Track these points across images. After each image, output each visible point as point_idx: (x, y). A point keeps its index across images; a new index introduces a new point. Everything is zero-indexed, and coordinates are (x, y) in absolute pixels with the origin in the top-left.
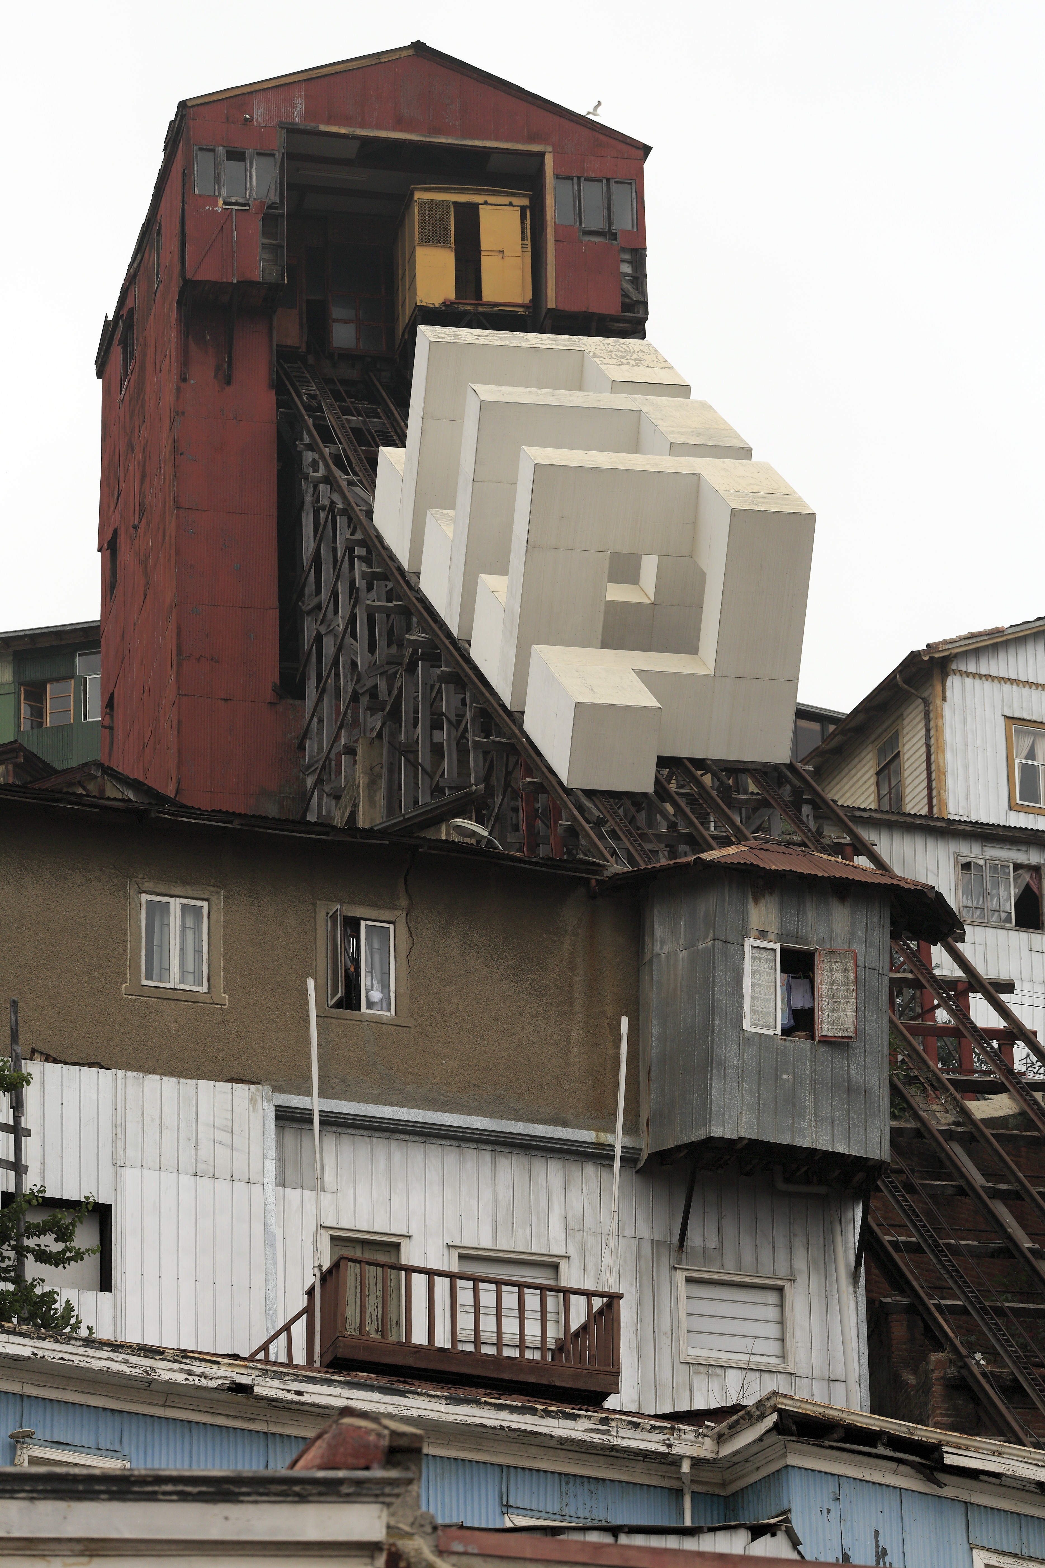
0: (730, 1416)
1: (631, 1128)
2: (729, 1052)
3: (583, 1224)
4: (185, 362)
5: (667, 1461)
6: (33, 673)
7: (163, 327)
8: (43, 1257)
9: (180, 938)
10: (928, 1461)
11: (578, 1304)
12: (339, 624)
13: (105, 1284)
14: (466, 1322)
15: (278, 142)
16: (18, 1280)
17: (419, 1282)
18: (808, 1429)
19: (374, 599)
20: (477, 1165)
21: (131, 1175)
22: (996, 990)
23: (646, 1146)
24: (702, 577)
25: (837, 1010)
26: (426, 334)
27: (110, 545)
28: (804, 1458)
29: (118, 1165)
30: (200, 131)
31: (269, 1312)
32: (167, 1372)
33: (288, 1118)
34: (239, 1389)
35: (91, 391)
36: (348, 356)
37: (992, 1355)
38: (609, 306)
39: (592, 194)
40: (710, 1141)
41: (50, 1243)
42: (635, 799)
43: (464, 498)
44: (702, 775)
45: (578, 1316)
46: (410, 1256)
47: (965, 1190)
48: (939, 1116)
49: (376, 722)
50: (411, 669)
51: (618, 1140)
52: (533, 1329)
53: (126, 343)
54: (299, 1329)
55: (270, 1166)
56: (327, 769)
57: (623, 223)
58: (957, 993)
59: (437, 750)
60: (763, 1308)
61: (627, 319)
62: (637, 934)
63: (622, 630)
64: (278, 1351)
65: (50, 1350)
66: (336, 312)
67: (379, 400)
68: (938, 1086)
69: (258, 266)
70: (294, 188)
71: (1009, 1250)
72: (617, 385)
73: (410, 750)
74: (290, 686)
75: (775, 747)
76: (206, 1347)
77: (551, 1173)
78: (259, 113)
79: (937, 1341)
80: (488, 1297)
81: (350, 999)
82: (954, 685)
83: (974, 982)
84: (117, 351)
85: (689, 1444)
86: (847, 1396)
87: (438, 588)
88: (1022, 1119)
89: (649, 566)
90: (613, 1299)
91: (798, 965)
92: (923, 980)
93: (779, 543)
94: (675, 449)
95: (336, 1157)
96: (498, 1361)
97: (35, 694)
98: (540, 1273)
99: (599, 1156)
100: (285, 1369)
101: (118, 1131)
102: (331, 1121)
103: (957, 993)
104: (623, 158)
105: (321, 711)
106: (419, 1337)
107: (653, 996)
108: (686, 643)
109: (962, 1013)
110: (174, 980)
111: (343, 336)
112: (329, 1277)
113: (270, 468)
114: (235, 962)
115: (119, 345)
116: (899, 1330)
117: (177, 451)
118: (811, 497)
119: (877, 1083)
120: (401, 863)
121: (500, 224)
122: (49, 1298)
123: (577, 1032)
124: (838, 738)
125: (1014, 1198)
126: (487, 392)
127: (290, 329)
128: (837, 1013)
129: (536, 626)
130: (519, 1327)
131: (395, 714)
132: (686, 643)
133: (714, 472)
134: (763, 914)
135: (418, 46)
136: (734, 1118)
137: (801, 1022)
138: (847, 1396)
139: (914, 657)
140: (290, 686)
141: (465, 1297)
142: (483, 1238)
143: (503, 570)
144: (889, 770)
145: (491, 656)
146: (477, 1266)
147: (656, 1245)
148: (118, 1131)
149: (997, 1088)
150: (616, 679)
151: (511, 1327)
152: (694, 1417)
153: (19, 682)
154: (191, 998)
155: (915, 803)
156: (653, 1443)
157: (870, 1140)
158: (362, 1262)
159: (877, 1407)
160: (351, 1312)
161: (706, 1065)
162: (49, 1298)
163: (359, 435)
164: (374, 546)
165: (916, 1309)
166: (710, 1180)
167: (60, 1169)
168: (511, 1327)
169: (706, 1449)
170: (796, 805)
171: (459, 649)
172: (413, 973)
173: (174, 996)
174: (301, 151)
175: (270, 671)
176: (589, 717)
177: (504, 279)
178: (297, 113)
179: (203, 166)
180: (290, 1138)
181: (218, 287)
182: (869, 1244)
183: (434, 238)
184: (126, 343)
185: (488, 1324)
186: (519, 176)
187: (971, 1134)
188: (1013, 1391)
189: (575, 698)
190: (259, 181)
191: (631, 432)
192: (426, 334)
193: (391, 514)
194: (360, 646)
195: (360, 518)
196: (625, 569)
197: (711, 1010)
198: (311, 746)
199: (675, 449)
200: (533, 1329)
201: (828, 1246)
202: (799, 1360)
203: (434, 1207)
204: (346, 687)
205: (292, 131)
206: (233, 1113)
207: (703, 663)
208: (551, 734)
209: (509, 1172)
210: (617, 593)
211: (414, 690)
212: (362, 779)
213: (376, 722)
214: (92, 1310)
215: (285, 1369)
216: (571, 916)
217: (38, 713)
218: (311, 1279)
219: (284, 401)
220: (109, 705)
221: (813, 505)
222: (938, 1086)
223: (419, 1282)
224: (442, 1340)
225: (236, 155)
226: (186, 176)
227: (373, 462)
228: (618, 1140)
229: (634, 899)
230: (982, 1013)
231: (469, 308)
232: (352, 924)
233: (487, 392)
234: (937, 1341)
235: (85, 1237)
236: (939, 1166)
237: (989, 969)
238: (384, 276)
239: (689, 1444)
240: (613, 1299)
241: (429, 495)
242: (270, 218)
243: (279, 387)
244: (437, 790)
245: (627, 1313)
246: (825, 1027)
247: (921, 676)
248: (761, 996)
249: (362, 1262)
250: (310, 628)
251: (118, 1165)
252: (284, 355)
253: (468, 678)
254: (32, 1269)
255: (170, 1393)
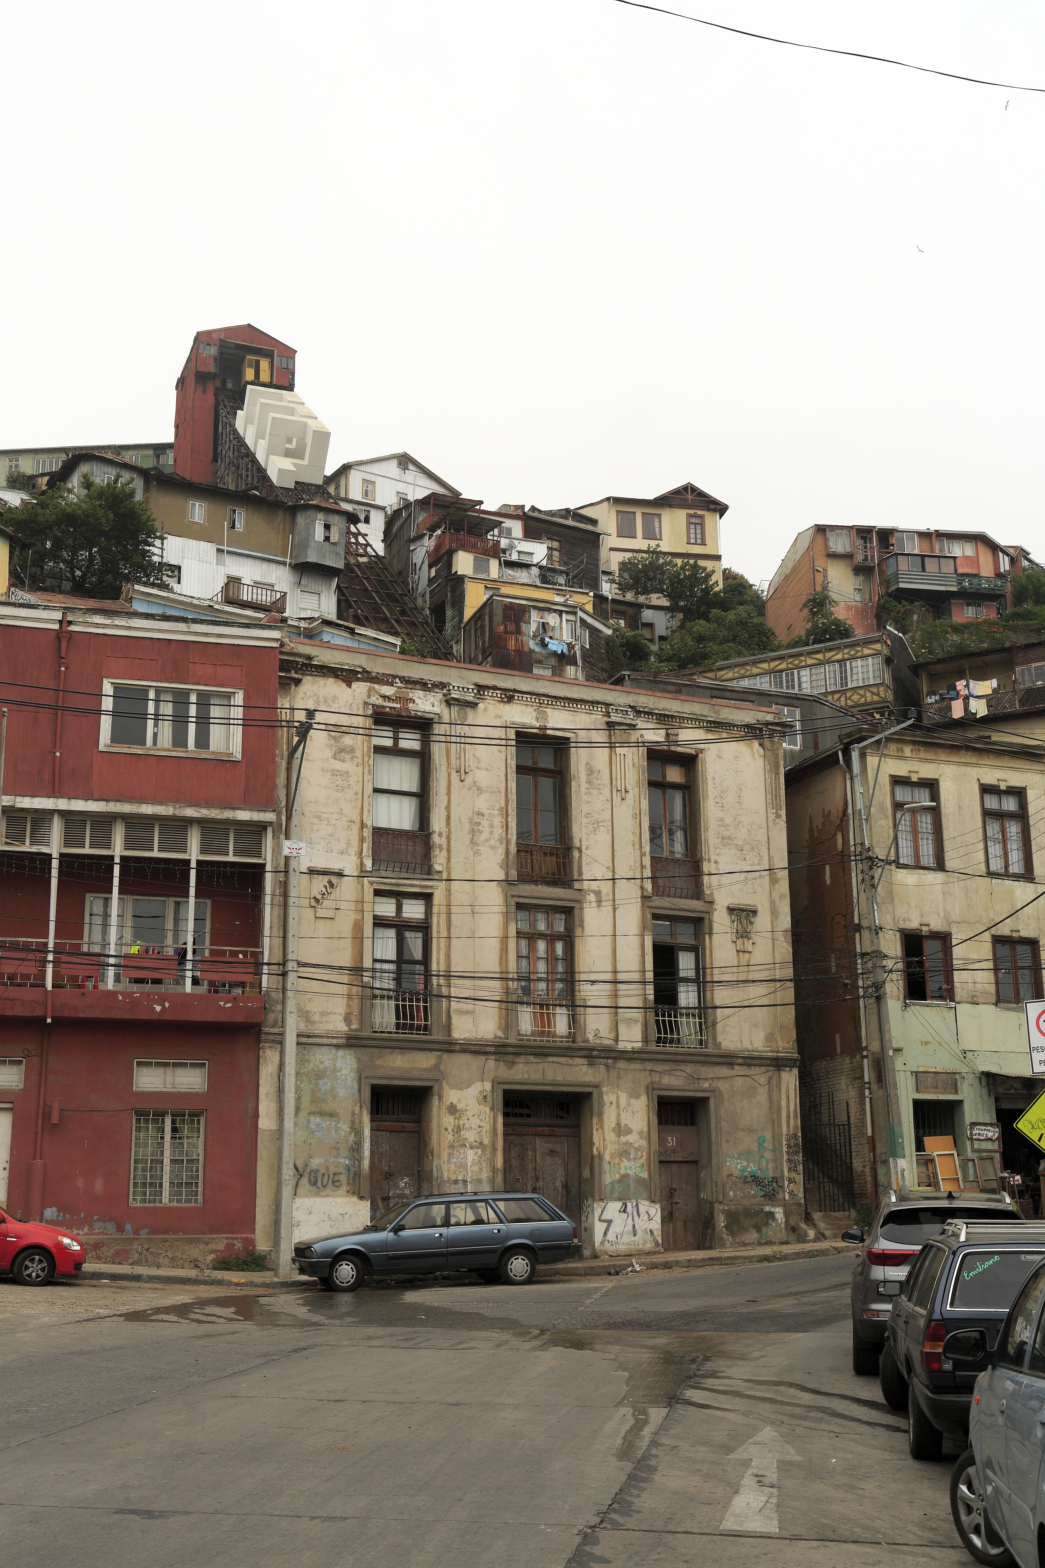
0: (311, 619)
1: (291, 558)
2: (312, 544)
3: (280, 578)
4: (196, 388)
5: (299, 628)
6: (158, 452)
7: (191, 380)
8: (168, 576)
9: (198, 511)
10: (352, 631)
11: (278, 594)
12: (226, 447)
13: (179, 583)
14: (255, 596)
15: (218, 343)
16: (162, 580)
17: (245, 587)
18: (327, 623)
19: (235, 442)
20: (258, 563)
21: (185, 560)
22: (364, 536)
23: (294, 562)
24: (306, 444)
25: (335, 537)
26: (249, 387)
27: (177, 426)
28: (326, 629)
29: (183, 558)
30: (201, 339)
31: (213, 591)
32: (195, 602)
33: (218, 550)
34: (210, 606)
35: (174, 393)
36: (230, 390)
37: (362, 611)
38: (287, 384)
39: (284, 360)
40: (307, 562)
41: (169, 573)
42: (290, 489)
43: (256, 423)
44: (118, 477)
45: (278, 596)
46: (243, 581)
47: (357, 576)
48: (352, 561)
49: (234, 468)
50: (242, 458)
51: (288, 561)
52: (269, 599)
53: (183, 383)
54: (220, 595)
55: (215, 560)
56: (222, 478)
57: (290, 367)
58: (356, 536)
59: (247, 476)
60: (316, 597)
61: (290, 387)
62: (294, 517)
63: (288, 454)
64: (215, 599)
65: (171, 595)
66: (228, 380)
67: (238, 399)
68: (352, 554)
69: (213, 369)
70: (221, 353)
71: (366, 589)
72: (289, 402)
73: (241, 475)
74: (215, 460)
75: (320, 481)
76: (203, 597)
77: (273, 566)
78: (214, 336)
79: (351, 607)
80: (260, 591)
81: (233, 527)
82: (352, 471)
83: (360, 533)
84: (180, 384)
85: (303, 624)
86: (332, 616)
87: (249, 441)
88: (369, 563)
89: (295, 441)
90: (286, 593)
91: (327, 527)
92: (349, 532)
93: (322, 438)
94: (301, 416)
95: (228, 559)
96: (261, 604)
97: (158, 457)
98: (271, 587)
99: (284, 564)
100: (217, 603)
101: (183, 550)
102: (228, 552)
103: (356, 536)
104: (289, 353)
105: (222, 466)
106: (245, 598)
107: (297, 531)
108: (302, 458)
109: (357, 539)
110: (196, 520)
111: (229, 385)
112: (227, 584)
113: (213, 413)
114: (209, 517)
115: (181, 384)
116: (343, 604)
117: (193, 407)
118: (330, 429)
119: (342, 553)
120: (241, 498)
121: (264, 364)
122: (168, 585)
123: (280, 538)
124: (329, 480)
125: (367, 579)
126: (262, 401)
127: (218, 383)
128: (334, 538)
129: (270, 451)
130: (265, 598)
131: (238, 467)
132: (302, 458)
133: (310, 422)
134: (320, 516)
135: (249, 325)
136: (312, 558)
137: (327, 539)
138: (332, 616)
139: (344, 465)
140: (215, 460)
141: (255, 591)
142: (259, 579)
143: (264, 439)
144: (337, 488)
145: (260, 457)
146: (257, 585)
147: (295, 583)
148: (183, 550)
149: (364, 556)
150: (287, 464)
151: (264, 598)
152: (304, 619)
153: (155, 454)
154: (200, 524)
155: (343, 495)
156: (296, 624)
157: (340, 565)
158: (233, 582)
159: (338, 618)
160: (231, 592)
161: (307, 546)
162: (168, 585)
163: (232, 407)
164: (235, 431)
165: (347, 600)
166: (306, 570)
167: (171, 558)
168: (264, 598)
169: (306, 626)
170: (324, 493)
171: (253, 455)
172: (246, 522)
173: (196, 523)
174: (223, 346)
175: (211, 457)
176: (281, 471)
177: (265, 377)
178: (222, 337)
179: (201, 346)
180: (219, 555)
181: (203, 373)
182: (338, 586)
183: (250, 366)
184: (183, 383)
185: (259, 597)
186: (269, 355)
187: (359, 565)
188: (366, 618)
189: (279, 468)
190: (213, 351)
191: (292, 412)
192: (249, 387)
193: (239, 425)
194: (231, 453)
195: (233, 425)
196: (289, 441)
197: (309, 535)
198: (219, 473)
199: (301, 416)
200: (269, 599)
201: (330, 586)
202: (322, 609)
203: (250, 572)
204: (227, 461)
205: (221, 340)
206: (208, 549)
207: (306, 462)
208: (273, 475)
209: (265, 565)
210: (288, 446)
211: (243, 463)
212: (230, 481)
213: (234, 468)
214: (176, 587)
215: (217, 603)
216: (280, 513)
217: (158, 461)
218: (223, 585)
219: (216, 399)
220: (175, 461)
221: (330, 431)
222: (352, 554)
223: (245, 587)
224: (250, 600)
225: (209, 345)
226: (198, 348)
227: (235, 414)
228: (288, 561)
229: (294, 510)
230: (361, 540)
231: (256, 382)
232: (234, 511)
233: (262, 401)
234: (351, 607)
235: (176, 573)
236: (352, 571)
237: (362, 531)
238: (239, 374)
239: (303, 624)
240: (286, 593)
241: (248, 421)
242: (215, 359)
243: (215, 395)
244: (247, 485)
245: (288, 596)
246: (332, 541)
247: (345, 469)
248: (319, 533)
249: (233, 582)
250: (220, 448)
251: (183, 558)
252: (217, 389)
253: (255, 461)
254: (165, 578)
255: (196, 606)
